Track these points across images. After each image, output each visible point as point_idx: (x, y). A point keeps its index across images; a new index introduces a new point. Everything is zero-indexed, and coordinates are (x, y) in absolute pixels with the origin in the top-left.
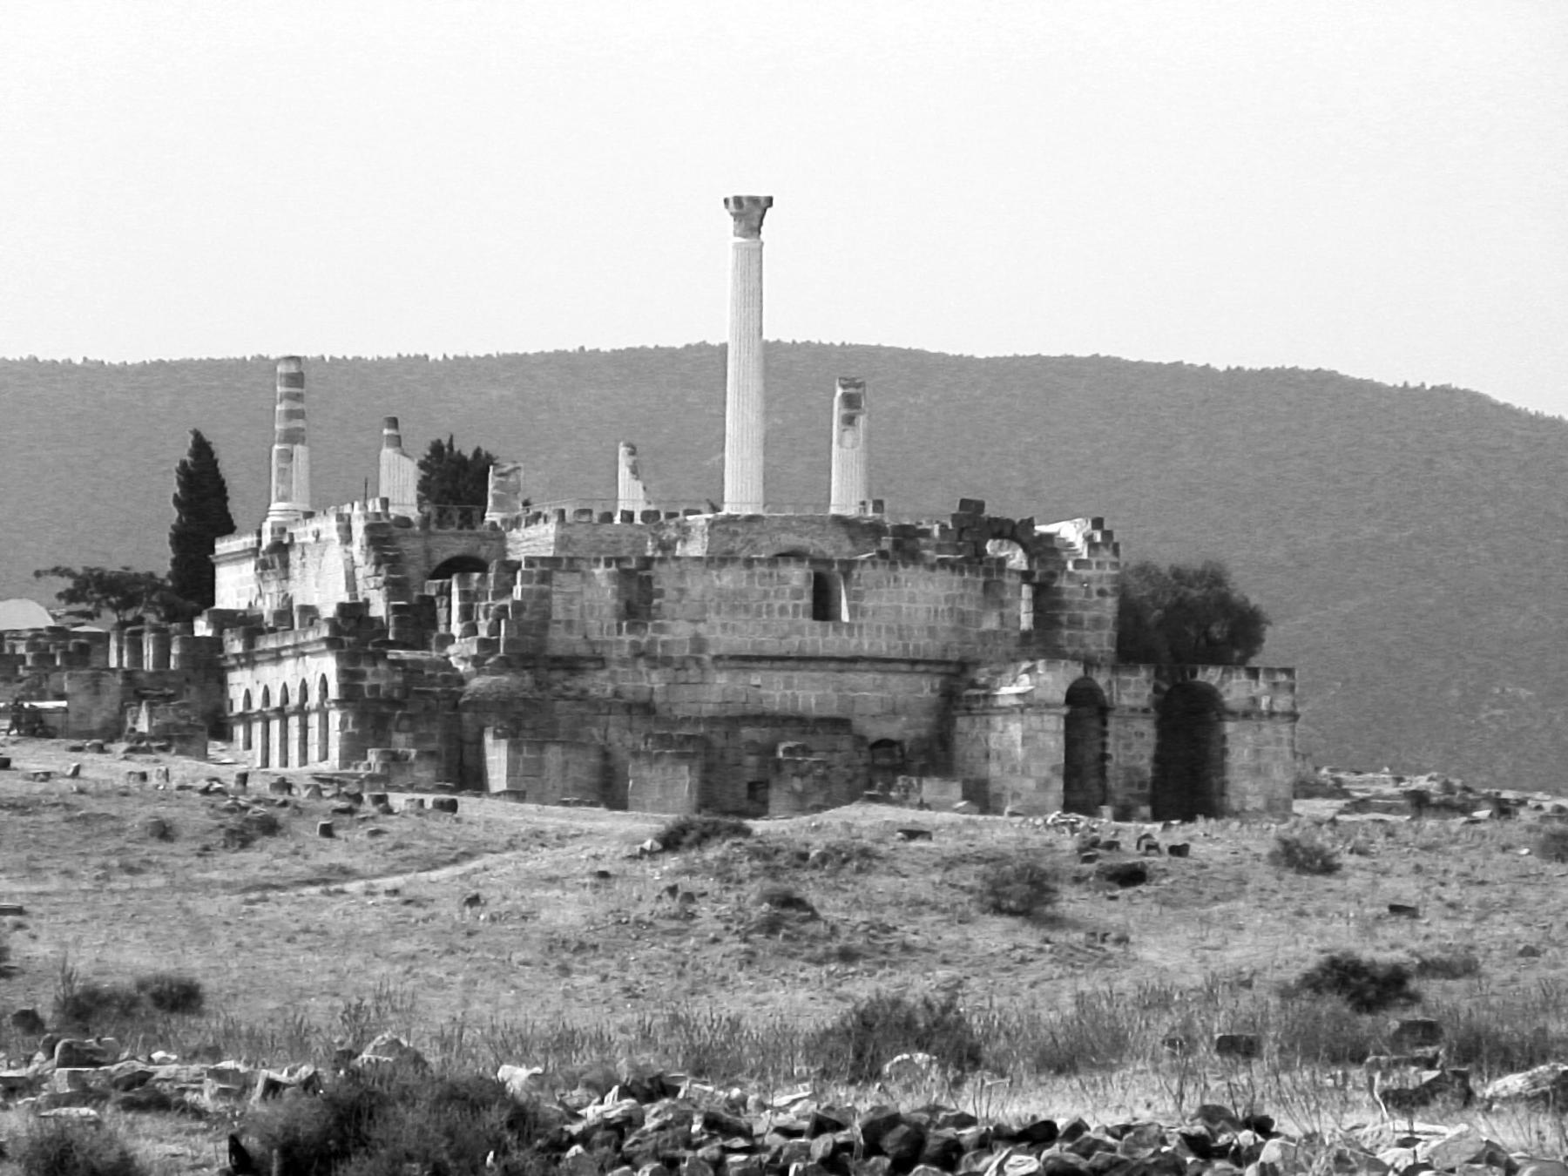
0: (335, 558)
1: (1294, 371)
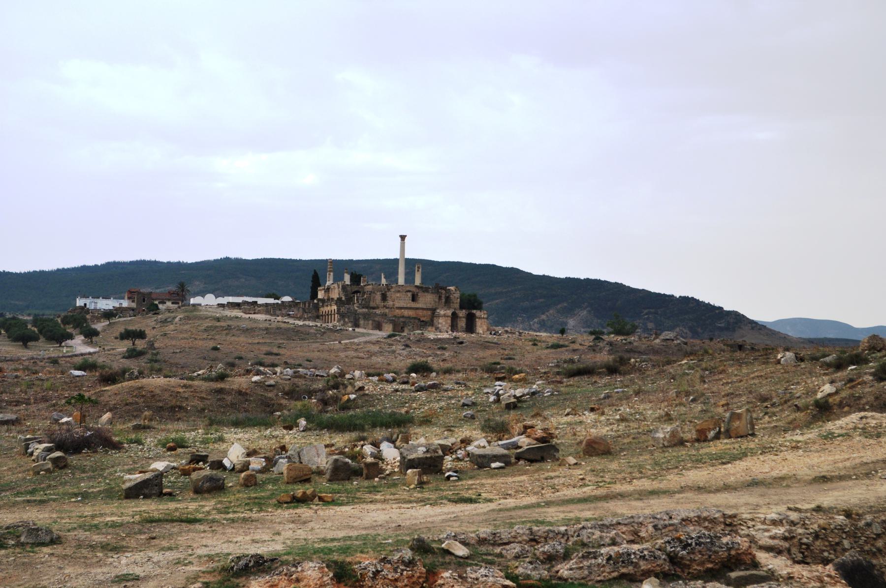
0: (336, 291)
1: (144, 261)
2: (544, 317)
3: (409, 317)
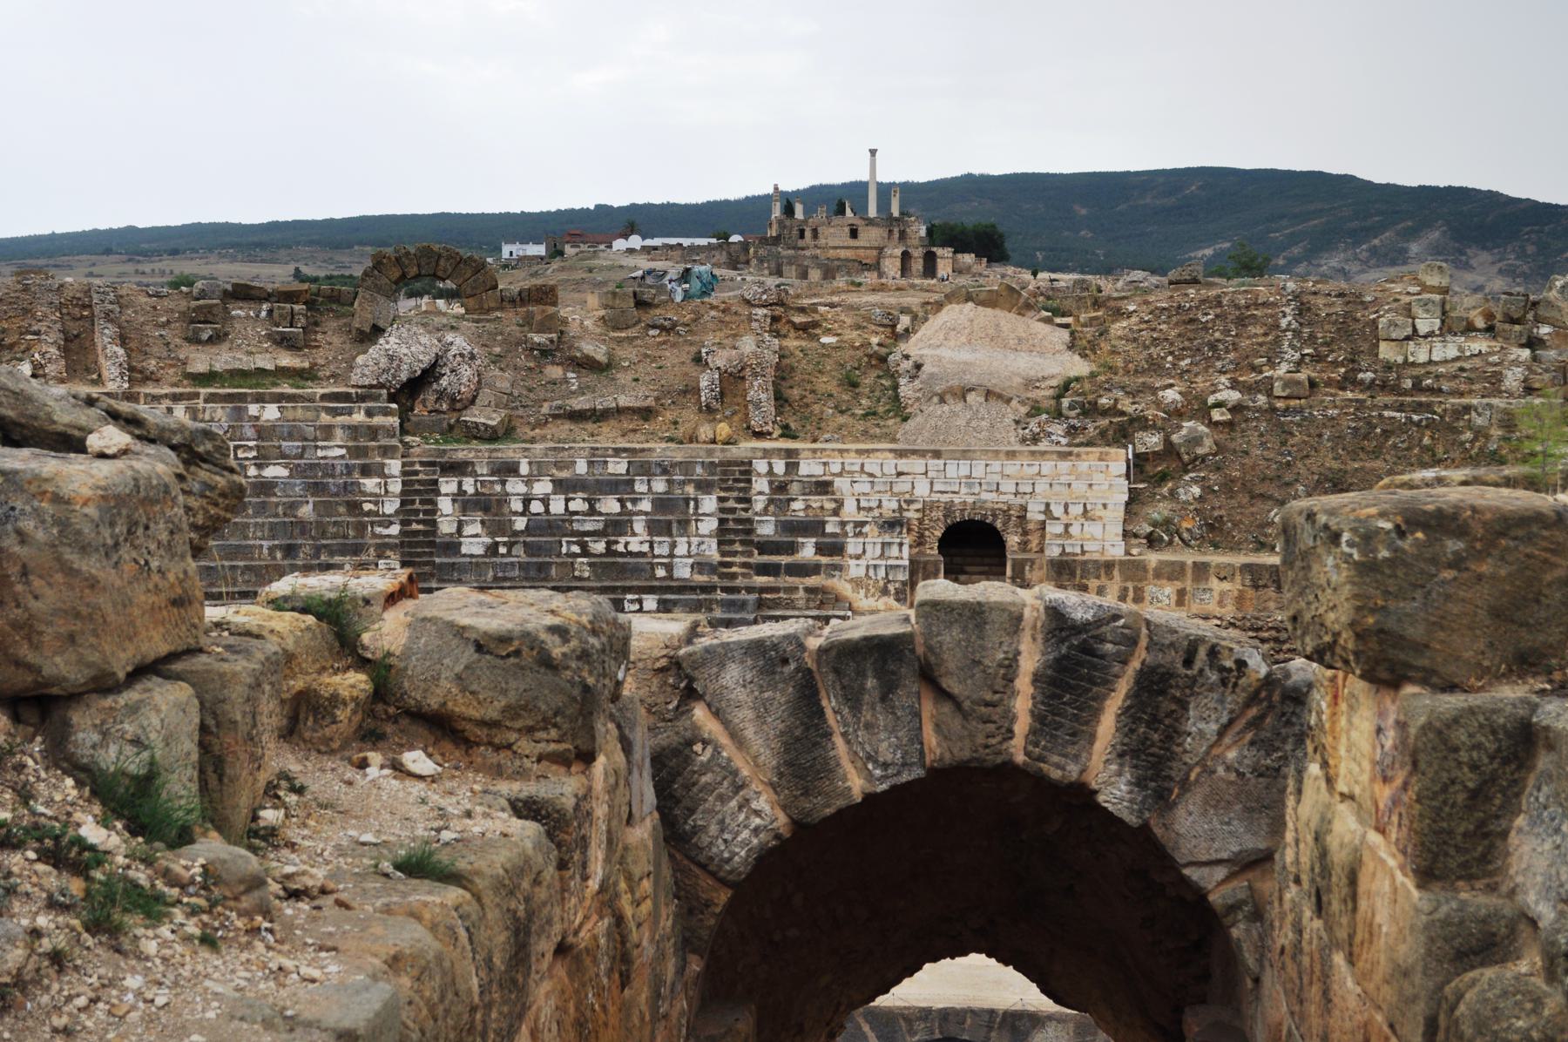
2: (1376, 242)
3: (847, 260)
